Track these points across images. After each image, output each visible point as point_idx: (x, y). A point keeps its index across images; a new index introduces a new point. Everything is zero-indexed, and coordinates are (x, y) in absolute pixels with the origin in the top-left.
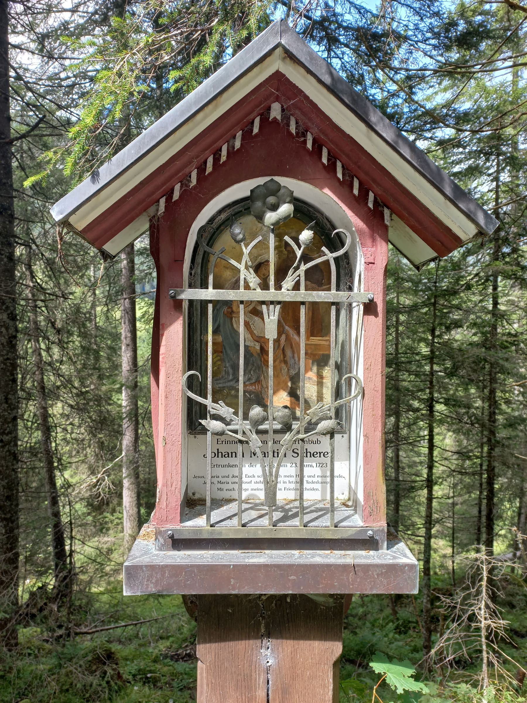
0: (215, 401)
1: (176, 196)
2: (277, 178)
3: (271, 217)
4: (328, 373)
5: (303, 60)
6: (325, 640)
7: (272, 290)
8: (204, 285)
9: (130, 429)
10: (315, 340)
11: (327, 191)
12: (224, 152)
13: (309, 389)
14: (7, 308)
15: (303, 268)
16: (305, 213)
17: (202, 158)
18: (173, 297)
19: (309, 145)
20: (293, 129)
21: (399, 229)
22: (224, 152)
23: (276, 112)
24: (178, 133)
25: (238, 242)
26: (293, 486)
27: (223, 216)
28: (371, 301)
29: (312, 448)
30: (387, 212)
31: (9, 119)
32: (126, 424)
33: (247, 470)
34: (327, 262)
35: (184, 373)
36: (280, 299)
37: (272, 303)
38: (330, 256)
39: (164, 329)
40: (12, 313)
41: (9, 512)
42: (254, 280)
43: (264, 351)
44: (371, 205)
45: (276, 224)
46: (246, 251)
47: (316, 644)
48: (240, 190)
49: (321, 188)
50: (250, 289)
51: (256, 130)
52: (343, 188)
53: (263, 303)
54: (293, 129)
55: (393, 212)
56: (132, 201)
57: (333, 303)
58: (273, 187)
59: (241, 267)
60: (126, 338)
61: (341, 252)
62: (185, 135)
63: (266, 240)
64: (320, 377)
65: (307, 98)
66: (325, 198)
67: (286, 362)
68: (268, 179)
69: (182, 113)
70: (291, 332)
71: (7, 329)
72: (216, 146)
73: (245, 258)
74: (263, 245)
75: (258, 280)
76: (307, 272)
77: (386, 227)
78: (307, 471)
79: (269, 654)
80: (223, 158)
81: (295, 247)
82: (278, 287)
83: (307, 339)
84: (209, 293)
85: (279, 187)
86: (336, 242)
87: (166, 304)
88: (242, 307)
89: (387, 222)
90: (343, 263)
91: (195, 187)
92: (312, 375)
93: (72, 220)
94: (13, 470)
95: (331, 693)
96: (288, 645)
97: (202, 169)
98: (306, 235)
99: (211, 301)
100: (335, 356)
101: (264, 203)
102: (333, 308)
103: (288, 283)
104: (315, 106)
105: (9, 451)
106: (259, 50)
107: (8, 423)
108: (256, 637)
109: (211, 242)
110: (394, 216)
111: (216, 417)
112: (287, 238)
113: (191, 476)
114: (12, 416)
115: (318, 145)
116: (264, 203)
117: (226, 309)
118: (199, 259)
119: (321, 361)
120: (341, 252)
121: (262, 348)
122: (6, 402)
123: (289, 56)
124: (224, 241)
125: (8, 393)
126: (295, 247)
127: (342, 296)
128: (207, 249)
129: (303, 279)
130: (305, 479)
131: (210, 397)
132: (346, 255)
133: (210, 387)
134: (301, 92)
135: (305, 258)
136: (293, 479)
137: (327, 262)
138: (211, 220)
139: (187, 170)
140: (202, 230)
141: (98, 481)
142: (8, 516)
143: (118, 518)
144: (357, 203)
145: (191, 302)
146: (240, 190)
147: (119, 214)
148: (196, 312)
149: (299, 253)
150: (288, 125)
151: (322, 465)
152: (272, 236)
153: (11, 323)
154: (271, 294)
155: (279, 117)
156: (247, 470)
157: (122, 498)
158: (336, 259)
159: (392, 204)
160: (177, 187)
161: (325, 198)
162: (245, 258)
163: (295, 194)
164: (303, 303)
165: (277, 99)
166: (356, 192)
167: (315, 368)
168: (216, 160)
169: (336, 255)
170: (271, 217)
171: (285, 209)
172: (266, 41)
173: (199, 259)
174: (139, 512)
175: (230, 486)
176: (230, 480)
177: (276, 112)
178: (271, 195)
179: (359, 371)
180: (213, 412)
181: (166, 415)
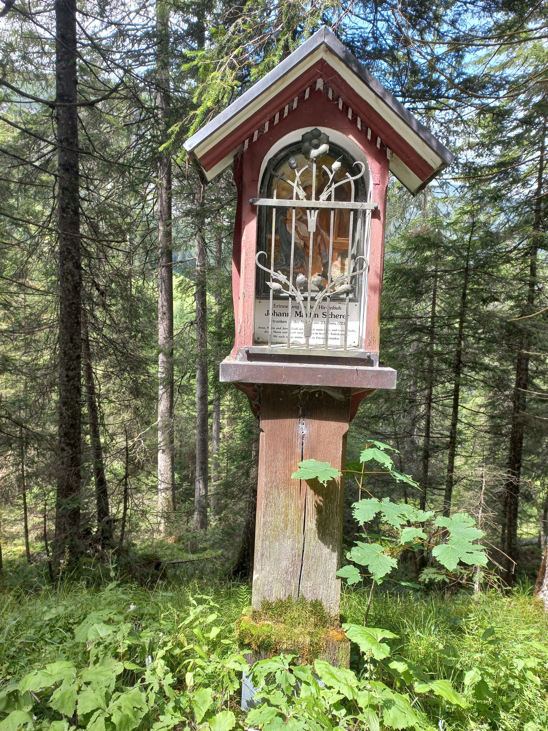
0: (276, 271)
1: (255, 138)
2: (319, 128)
3: (314, 153)
4: (349, 263)
5: (337, 52)
6: (339, 421)
7: (313, 200)
8: (270, 196)
9: (165, 396)
10: (340, 240)
11: (351, 137)
12: (286, 111)
13: (335, 272)
14: (73, 257)
15: (334, 186)
16: (336, 152)
17: (273, 114)
18: (252, 204)
19: (340, 107)
20: (330, 96)
21: (396, 163)
22: (286, 111)
23: (320, 84)
24: (260, 98)
25: (293, 169)
26: (322, 336)
27: (283, 154)
28: (376, 208)
29: (335, 312)
30: (389, 151)
31: (76, 83)
32: (161, 390)
33: (293, 325)
34: (349, 183)
35: (257, 252)
36: (318, 206)
37: (313, 208)
38: (351, 179)
39: (245, 225)
40: (76, 262)
41: (73, 438)
42: (302, 194)
43: (306, 246)
44: (378, 146)
45: (318, 157)
46: (298, 175)
47: (332, 423)
48: (294, 136)
49: (347, 134)
50: (299, 199)
51: (307, 96)
52: (361, 135)
53: (308, 208)
54: (330, 96)
55: (393, 151)
56: (230, 141)
57: (352, 210)
58: (315, 133)
59: (295, 185)
60: (162, 306)
61: (358, 176)
62: (264, 99)
63: (311, 167)
64: (343, 265)
65: (339, 76)
66: (350, 142)
67: (320, 254)
68: (313, 128)
69: (263, 85)
70: (325, 234)
71: (73, 276)
72: (281, 106)
73: (297, 179)
74: (308, 172)
75: (304, 194)
76: (336, 189)
77: (388, 161)
78: (331, 327)
79: (305, 428)
80: (286, 114)
81: (329, 173)
82: (317, 199)
83: (335, 238)
84: (274, 202)
85: (320, 133)
86: (355, 170)
87: (246, 209)
88: (294, 211)
89: (388, 158)
90: (360, 187)
91: (267, 133)
92: (338, 263)
93: (195, 151)
94: (77, 402)
95: (341, 453)
96: (316, 423)
97: (272, 121)
98: (336, 165)
99: (274, 207)
100: (352, 251)
101: (310, 144)
102: (352, 213)
103: (324, 196)
104: (344, 81)
105: (73, 385)
106: (311, 47)
107: (73, 360)
108: (297, 418)
109: (276, 168)
110: (394, 154)
111: (275, 281)
112: (324, 167)
113: (257, 327)
114: (76, 354)
115: (346, 107)
116: (310, 144)
117: (283, 211)
118: (266, 183)
119: (344, 254)
120: (358, 176)
121: (305, 244)
122: (72, 342)
123: (329, 49)
124: (285, 169)
125: (73, 334)
126: (329, 173)
127: (358, 205)
128: (273, 173)
129: (333, 194)
130: (329, 332)
131: (272, 268)
132: (362, 178)
133: (272, 261)
134: (336, 72)
135: (335, 181)
136: (323, 332)
137: (349, 183)
138: (276, 156)
139: (263, 122)
140: (270, 161)
141: (134, 445)
142: (73, 442)
143: (152, 481)
144: (370, 144)
145: (261, 207)
146: (294, 136)
147: (221, 149)
148: (264, 216)
149: (331, 177)
150: (327, 93)
151: (341, 323)
152: (315, 166)
153: (76, 271)
154: (313, 203)
155: (322, 88)
156: (293, 325)
157: (157, 463)
158: (356, 182)
159: (393, 147)
160: (256, 133)
161: (350, 142)
162: (297, 179)
163: (331, 139)
164: (333, 209)
165: (321, 77)
166: (369, 137)
167: (339, 259)
168: (281, 115)
169: (354, 178)
170: (314, 153)
171: (324, 148)
172: (315, 40)
173: (266, 183)
174: (173, 476)
175: (282, 335)
176: (282, 331)
177: (320, 84)
178: (314, 139)
179: (367, 257)
180: (274, 277)
181: (245, 279)
